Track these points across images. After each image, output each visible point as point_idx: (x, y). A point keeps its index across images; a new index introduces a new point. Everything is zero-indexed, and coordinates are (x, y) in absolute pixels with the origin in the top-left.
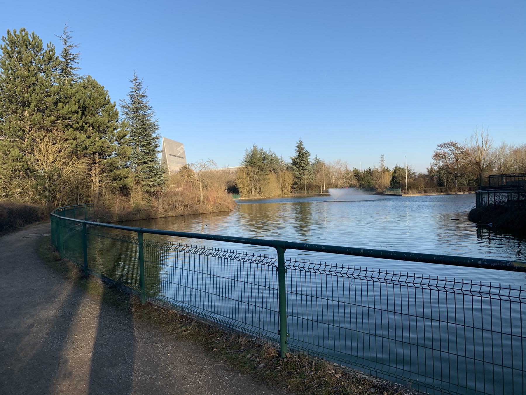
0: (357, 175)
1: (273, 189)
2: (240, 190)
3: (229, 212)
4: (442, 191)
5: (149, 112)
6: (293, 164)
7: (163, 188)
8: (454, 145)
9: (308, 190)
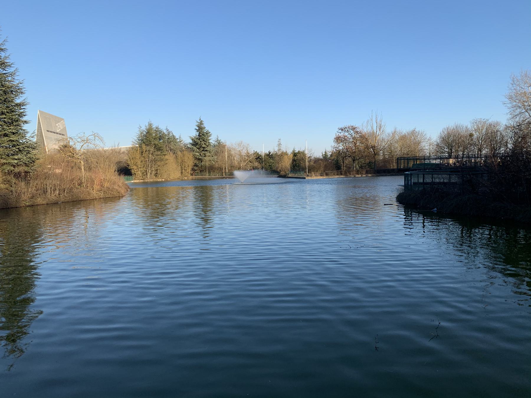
0: (258, 158)
1: (172, 170)
2: (133, 171)
3: (120, 197)
4: (341, 174)
5: (9, 70)
6: (192, 145)
7: (32, 168)
8: (354, 129)
9: (209, 172)
